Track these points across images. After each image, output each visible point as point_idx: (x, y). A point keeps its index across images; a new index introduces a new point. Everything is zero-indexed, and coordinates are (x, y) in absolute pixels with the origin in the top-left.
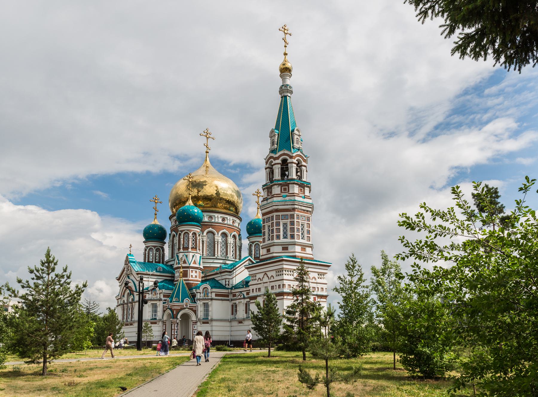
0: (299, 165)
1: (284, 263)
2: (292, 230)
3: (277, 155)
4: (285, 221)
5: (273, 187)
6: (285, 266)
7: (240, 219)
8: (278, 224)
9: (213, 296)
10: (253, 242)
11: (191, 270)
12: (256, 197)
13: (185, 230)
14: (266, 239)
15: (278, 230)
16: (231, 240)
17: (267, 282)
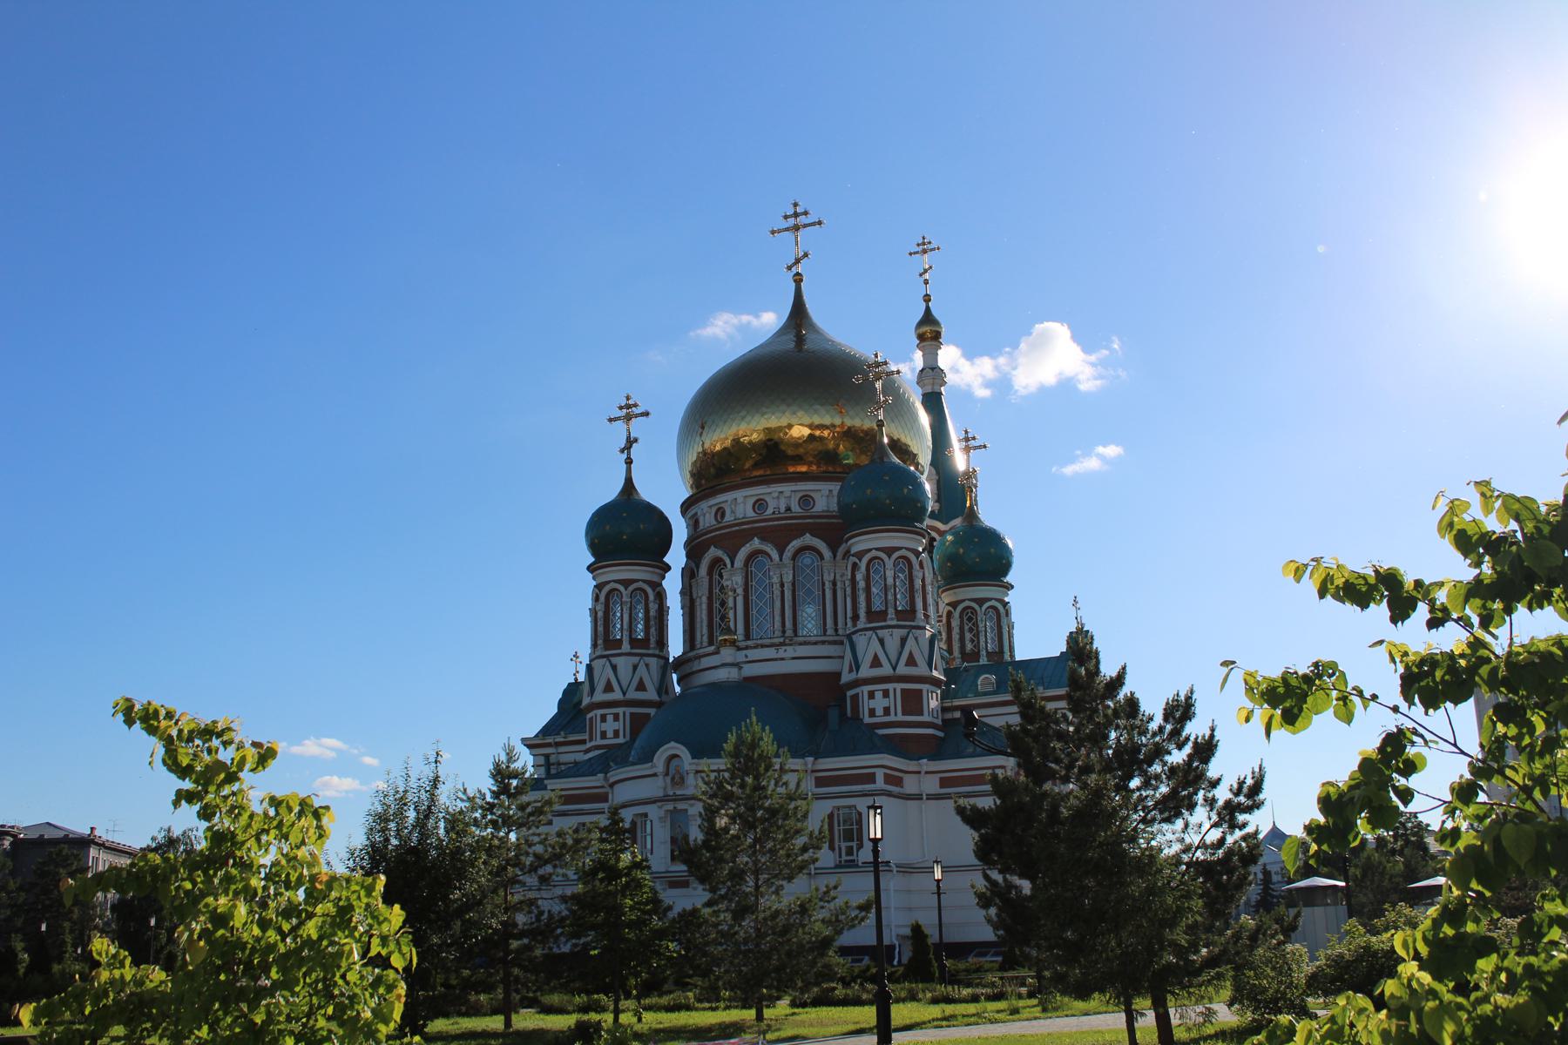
9: (809, 786)
11: (866, 689)
13: (870, 550)
17: (927, 773)
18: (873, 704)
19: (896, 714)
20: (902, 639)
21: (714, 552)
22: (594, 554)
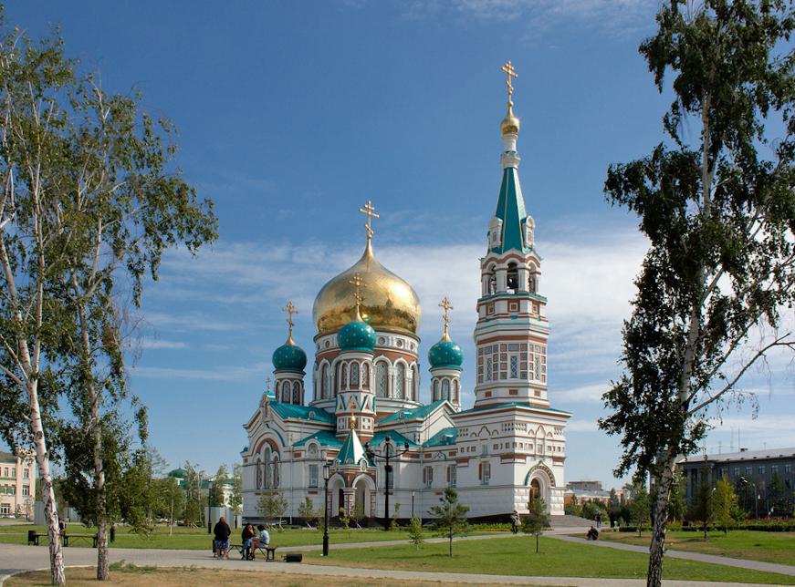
0: (533, 273)
1: (517, 413)
2: (524, 366)
3: (503, 256)
4: (514, 353)
6: (517, 418)
7: (418, 340)
8: (504, 357)
10: (440, 377)
11: (362, 417)
12: (443, 309)
16: (409, 374)
21: (324, 361)
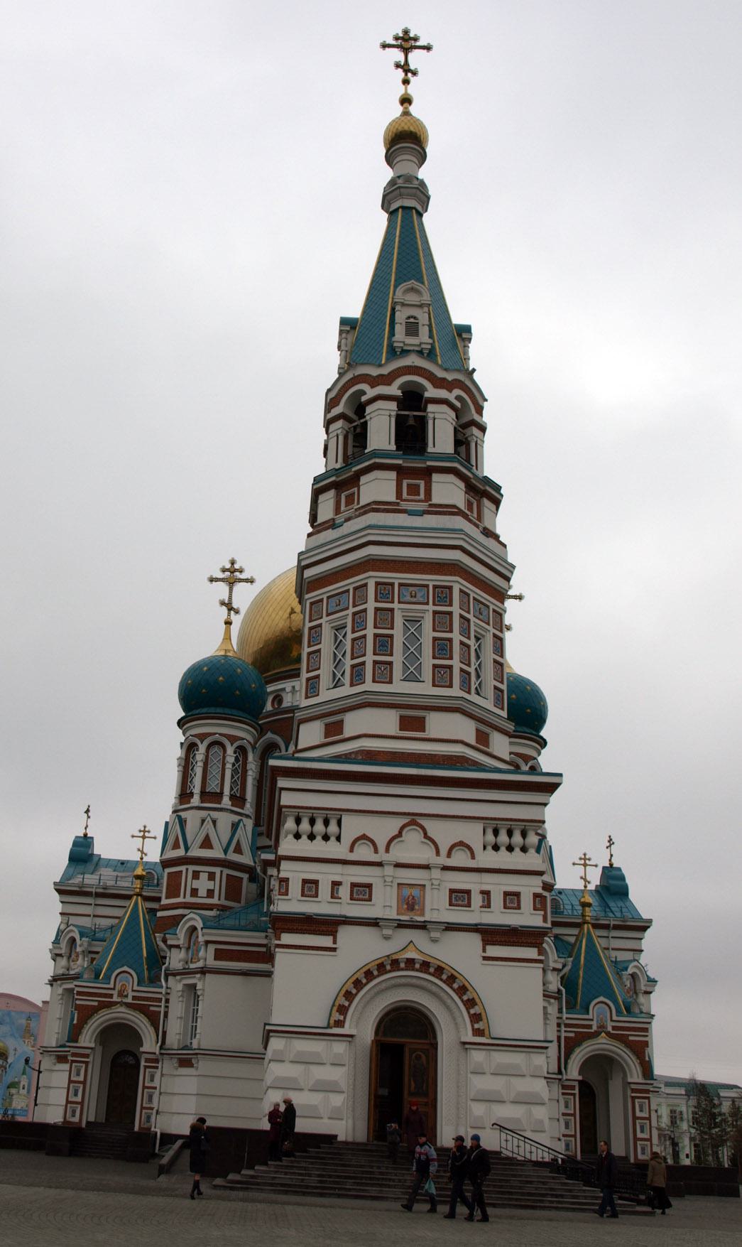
5: (363, 479)
8: (385, 616)
9: (207, 957)
11: (192, 868)
13: (215, 734)
14: (325, 681)
15: (384, 644)
18: (210, 885)
19: (184, 897)
20: (233, 825)
22: (184, 710)
